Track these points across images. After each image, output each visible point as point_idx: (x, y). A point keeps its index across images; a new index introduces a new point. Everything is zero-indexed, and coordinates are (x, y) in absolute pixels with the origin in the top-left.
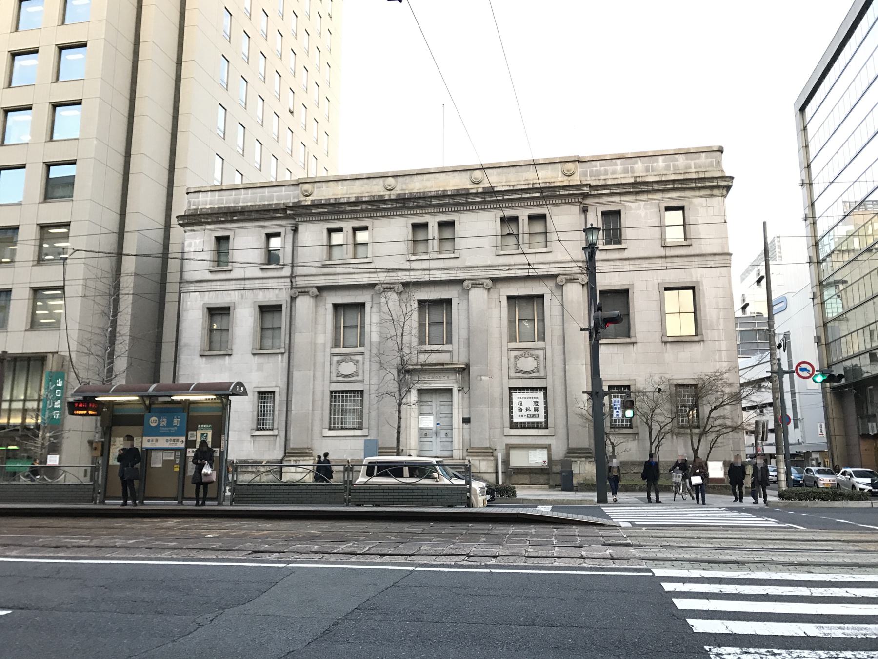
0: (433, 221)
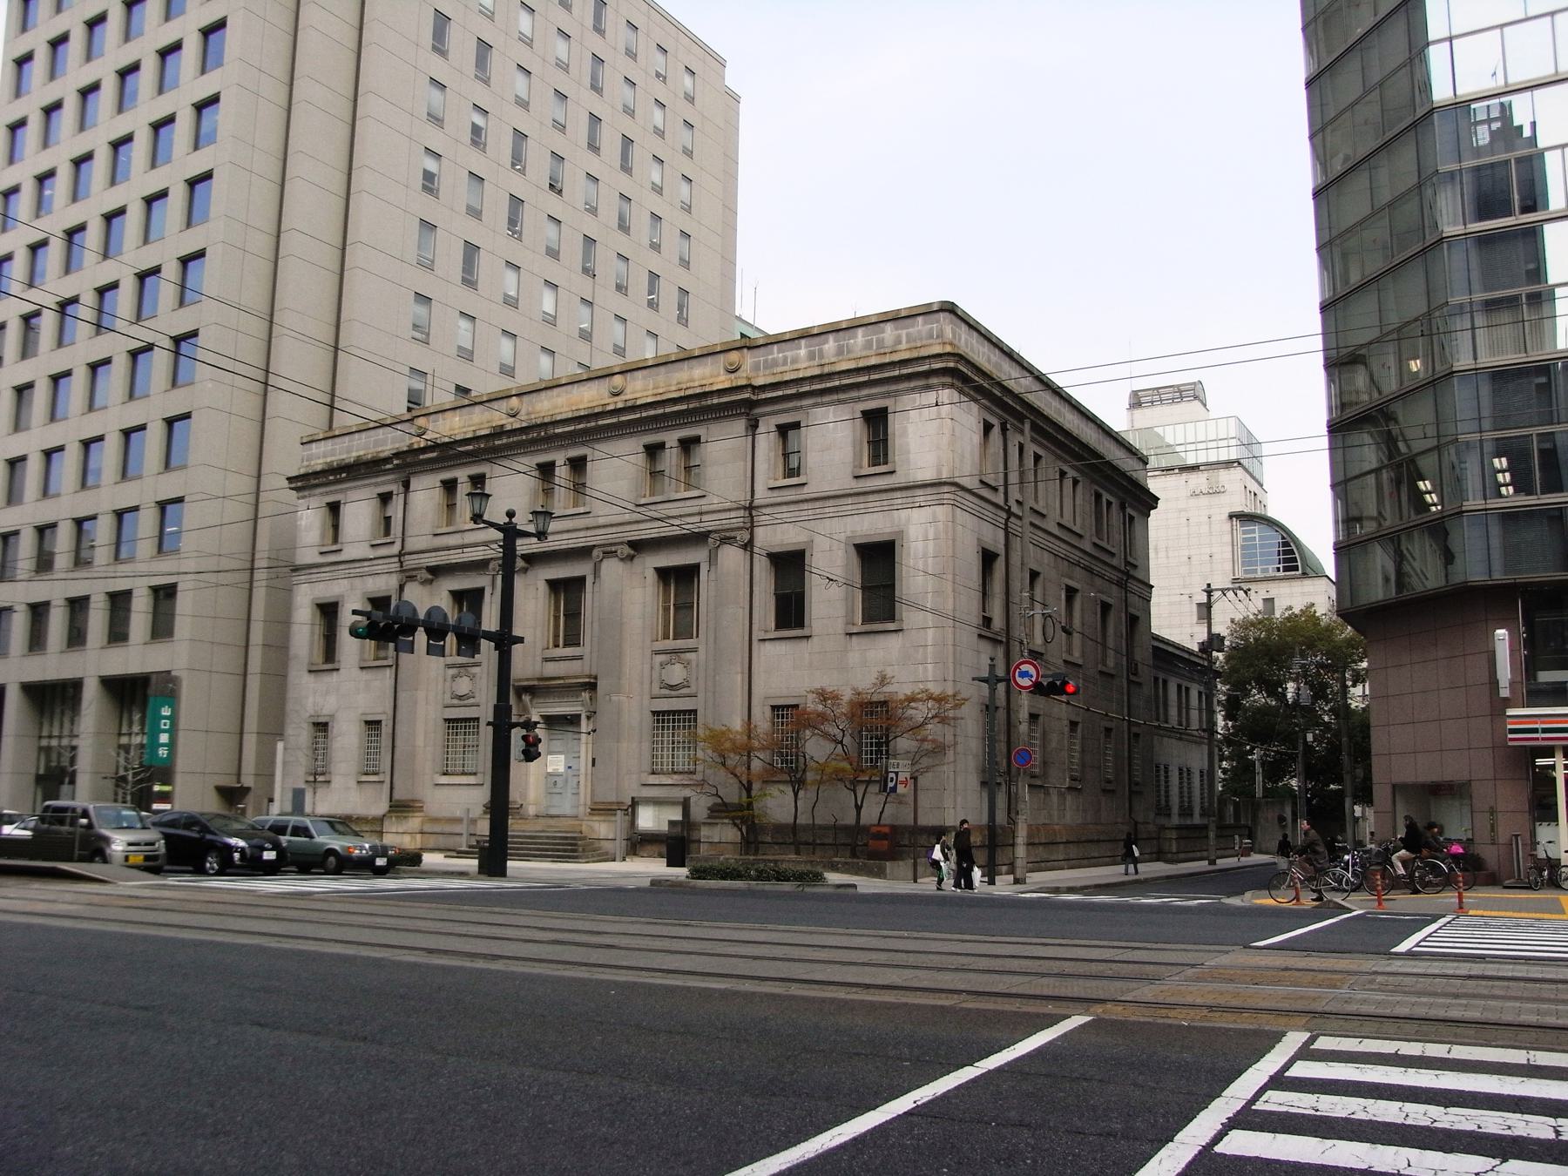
0: (671, 438)
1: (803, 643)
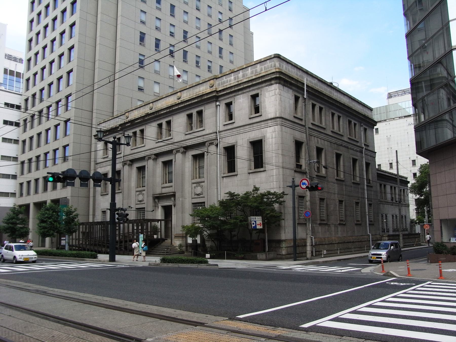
1: (235, 178)
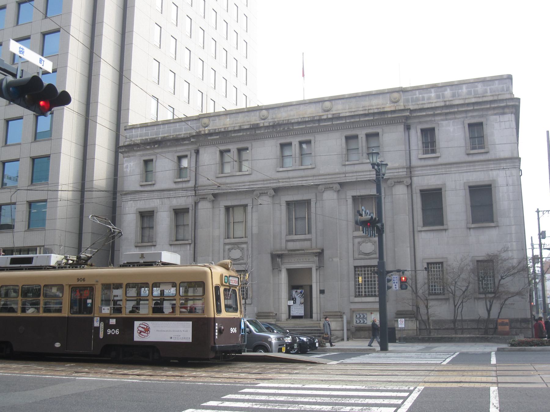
0: (233, 147)
1: (444, 234)
